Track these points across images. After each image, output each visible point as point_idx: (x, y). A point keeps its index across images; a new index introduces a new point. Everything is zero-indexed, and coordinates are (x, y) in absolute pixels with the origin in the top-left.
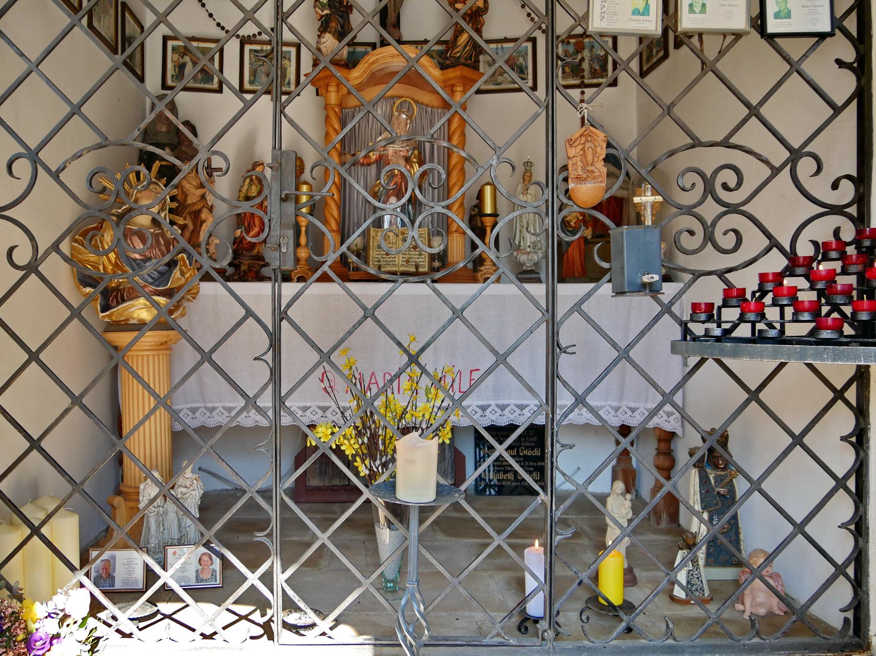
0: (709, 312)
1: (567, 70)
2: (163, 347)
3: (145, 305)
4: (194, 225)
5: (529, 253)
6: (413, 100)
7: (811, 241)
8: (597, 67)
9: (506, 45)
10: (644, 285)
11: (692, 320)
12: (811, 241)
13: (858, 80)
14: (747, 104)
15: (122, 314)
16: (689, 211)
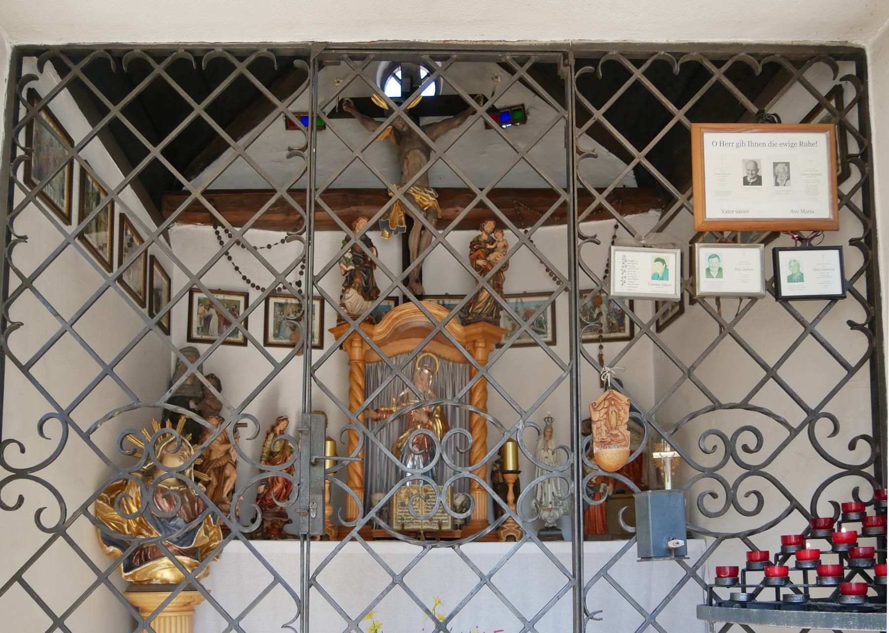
0: (733, 575)
2: (185, 608)
3: (168, 564)
4: (218, 480)
5: (550, 510)
6: (435, 354)
7: (830, 502)
8: (614, 322)
9: (525, 300)
10: (670, 550)
11: (717, 584)
12: (830, 502)
13: (870, 342)
14: (764, 366)
15: (145, 574)
16: (711, 473)
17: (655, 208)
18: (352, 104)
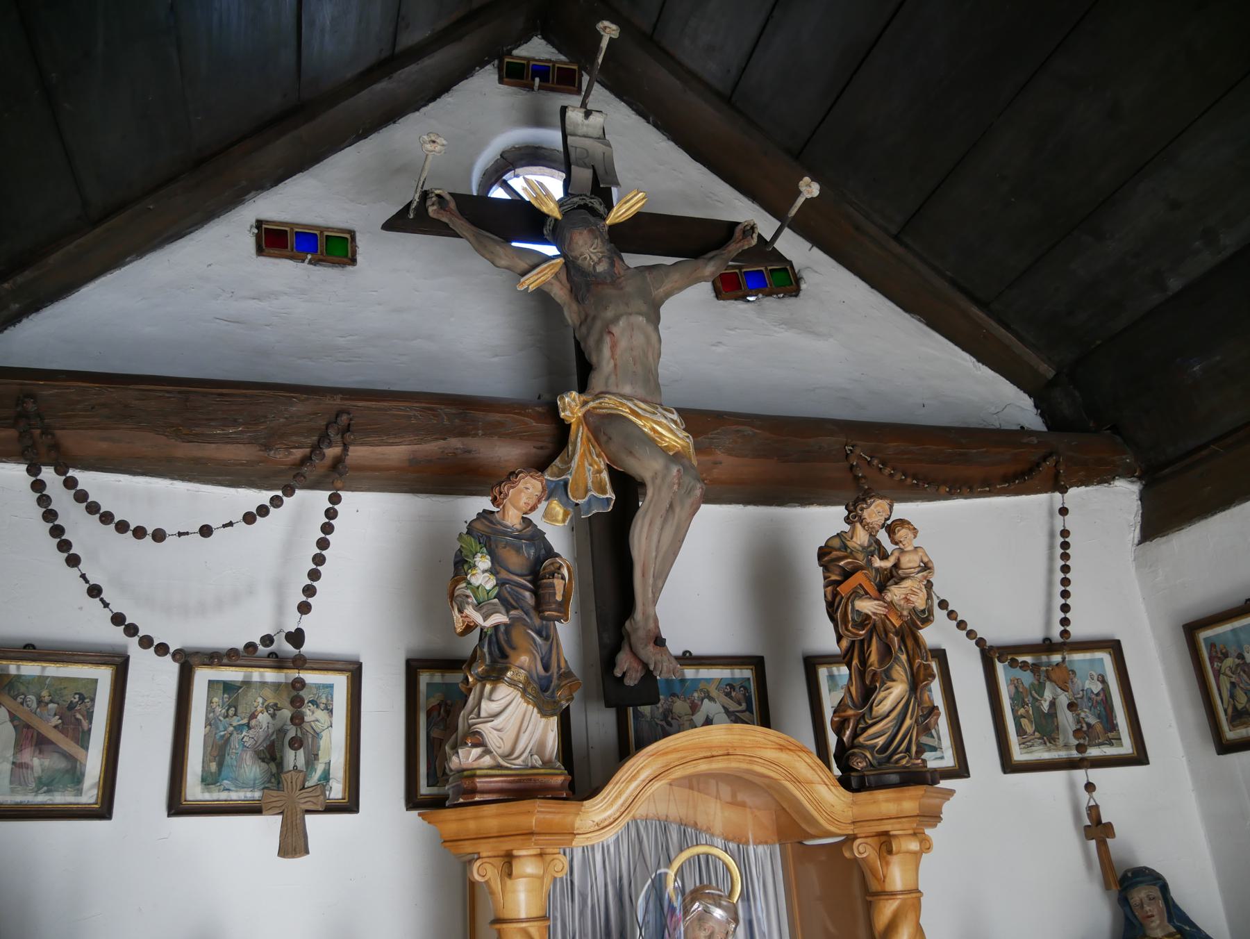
1: (1029, 728)
8: (1092, 720)
17: (1123, 475)
18: (452, 205)
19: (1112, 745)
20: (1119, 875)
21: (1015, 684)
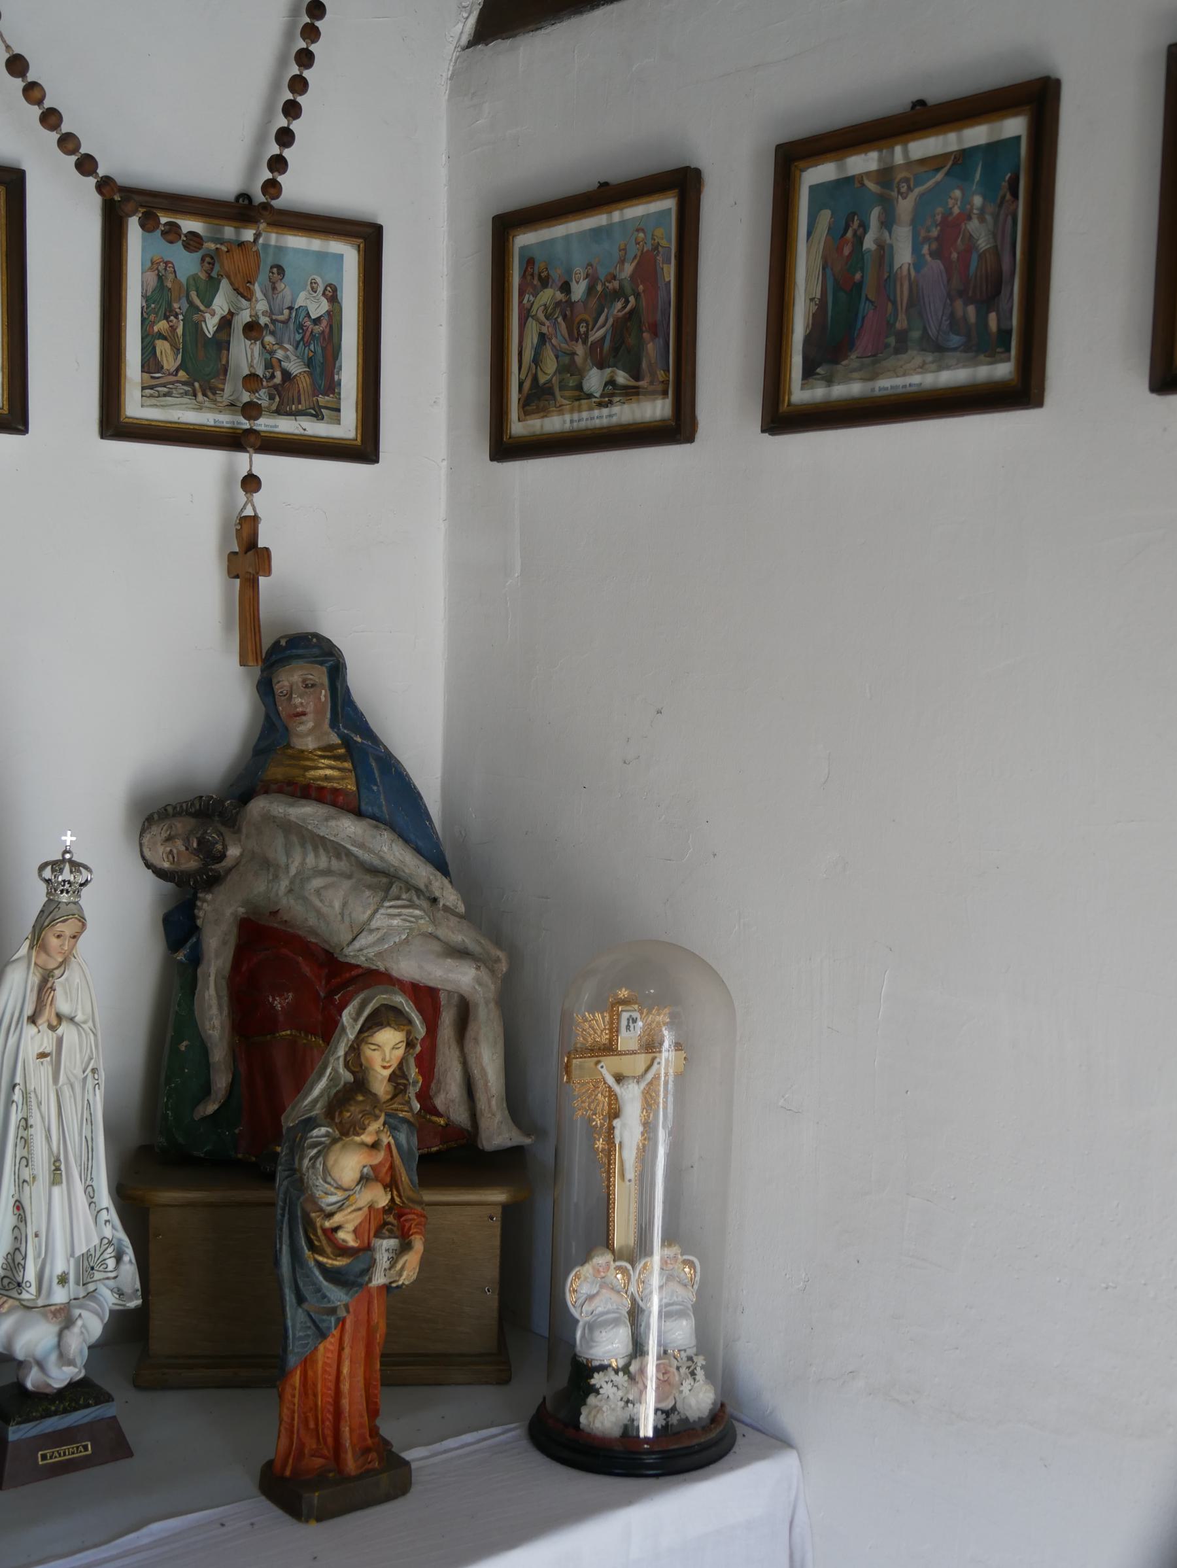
8: (295, 367)
19: (318, 416)
20: (267, 643)
21: (159, 270)
